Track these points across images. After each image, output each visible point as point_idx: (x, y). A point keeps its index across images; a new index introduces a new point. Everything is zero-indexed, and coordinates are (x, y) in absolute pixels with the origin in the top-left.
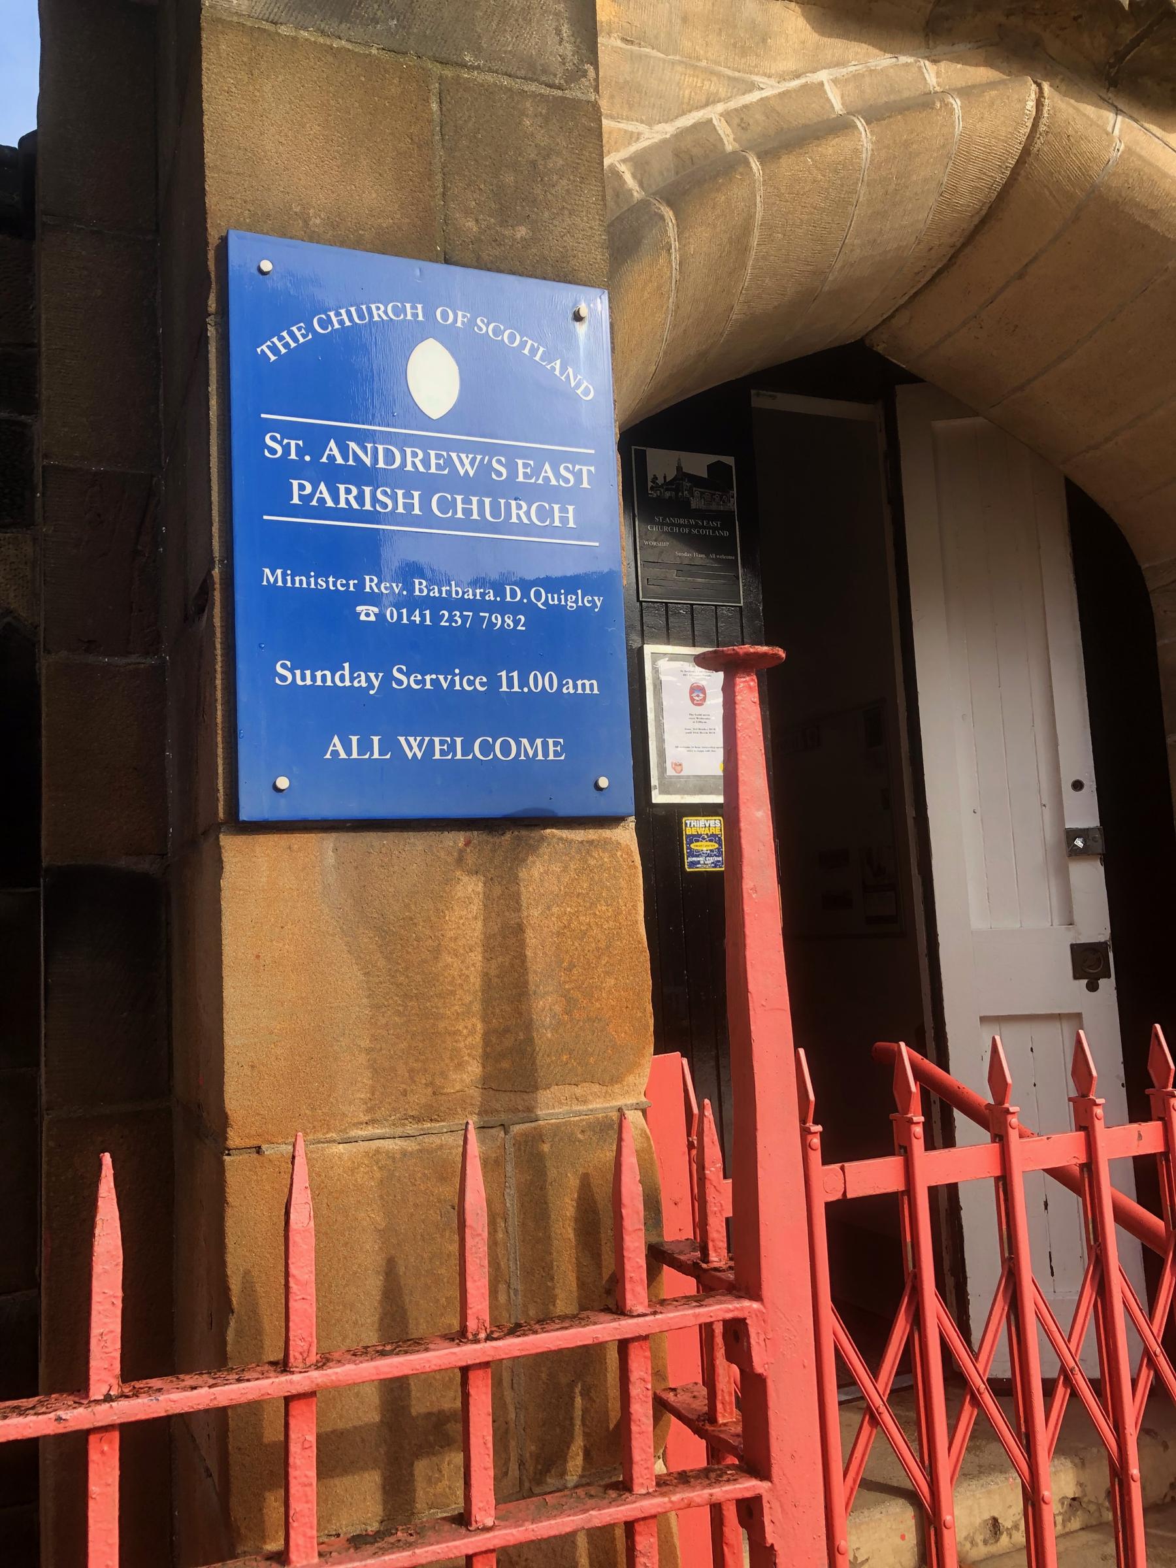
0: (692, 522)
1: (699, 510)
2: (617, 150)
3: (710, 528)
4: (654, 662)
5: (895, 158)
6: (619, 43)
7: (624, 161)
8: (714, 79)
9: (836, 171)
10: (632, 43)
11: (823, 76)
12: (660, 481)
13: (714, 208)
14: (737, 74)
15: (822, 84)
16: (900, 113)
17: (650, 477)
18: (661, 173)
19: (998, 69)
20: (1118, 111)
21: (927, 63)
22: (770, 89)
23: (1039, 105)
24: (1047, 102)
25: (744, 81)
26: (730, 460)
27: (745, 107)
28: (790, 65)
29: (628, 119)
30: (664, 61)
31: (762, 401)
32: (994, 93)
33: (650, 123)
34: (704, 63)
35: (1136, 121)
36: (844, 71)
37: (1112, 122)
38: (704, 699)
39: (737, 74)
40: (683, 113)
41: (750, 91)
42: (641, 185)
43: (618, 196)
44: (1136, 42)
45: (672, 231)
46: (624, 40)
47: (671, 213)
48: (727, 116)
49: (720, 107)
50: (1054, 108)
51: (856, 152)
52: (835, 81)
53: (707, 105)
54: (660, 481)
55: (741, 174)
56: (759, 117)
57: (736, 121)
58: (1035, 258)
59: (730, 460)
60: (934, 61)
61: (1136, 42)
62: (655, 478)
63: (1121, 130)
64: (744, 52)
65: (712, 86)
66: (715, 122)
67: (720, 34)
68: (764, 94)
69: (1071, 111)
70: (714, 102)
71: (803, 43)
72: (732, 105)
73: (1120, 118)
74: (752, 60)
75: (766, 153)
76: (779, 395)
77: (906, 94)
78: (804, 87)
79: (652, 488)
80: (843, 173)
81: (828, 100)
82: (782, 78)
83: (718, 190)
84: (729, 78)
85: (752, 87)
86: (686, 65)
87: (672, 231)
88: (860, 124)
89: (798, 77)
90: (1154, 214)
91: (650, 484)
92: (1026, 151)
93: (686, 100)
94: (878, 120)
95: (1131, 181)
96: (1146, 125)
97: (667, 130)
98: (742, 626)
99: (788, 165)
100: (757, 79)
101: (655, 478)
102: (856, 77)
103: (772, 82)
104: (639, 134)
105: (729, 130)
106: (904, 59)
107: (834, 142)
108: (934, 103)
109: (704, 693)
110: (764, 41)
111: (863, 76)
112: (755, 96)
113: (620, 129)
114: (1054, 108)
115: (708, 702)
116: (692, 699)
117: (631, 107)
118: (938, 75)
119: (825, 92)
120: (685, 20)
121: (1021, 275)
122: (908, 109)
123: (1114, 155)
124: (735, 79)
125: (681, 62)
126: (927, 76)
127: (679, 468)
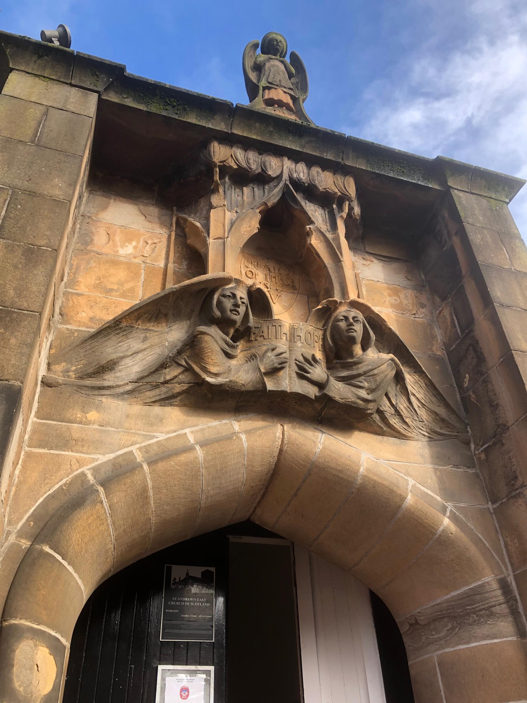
0: (191, 599)
1: (196, 594)
2: (87, 465)
3: (200, 602)
4: (162, 675)
5: (216, 458)
6: (97, 427)
7: (89, 469)
8: (137, 436)
9: (187, 465)
10: (103, 426)
11: (187, 431)
12: (177, 580)
13: (125, 484)
14: (147, 433)
15: (186, 434)
16: (217, 442)
17: (172, 578)
18: (105, 472)
19: (268, 421)
20: (323, 432)
21: (235, 422)
22: (162, 437)
23: (283, 434)
24: (286, 433)
25: (150, 436)
26: (213, 569)
27: (150, 445)
28: (173, 428)
29: (94, 453)
30: (115, 431)
31: (232, 539)
32: (261, 431)
33: (104, 454)
34: (133, 431)
35: (332, 436)
36: (196, 428)
37: (320, 438)
38: (188, 696)
39: (147, 433)
40: (120, 449)
41: (152, 439)
42: (95, 478)
43: (83, 483)
44: (323, 409)
45: (102, 495)
46: (100, 425)
47: (102, 489)
48: (140, 449)
49: (138, 446)
50: (289, 435)
51: (196, 458)
52: (192, 432)
53: (131, 445)
54: (177, 580)
55: (139, 471)
56: (155, 448)
57: (144, 450)
58: (299, 489)
59: (213, 569)
60: (238, 421)
61: (323, 409)
62: (175, 579)
63: (324, 440)
64: (152, 425)
65: (134, 439)
66: (134, 451)
67: (142, 419)
68: (158, 439)
69: (297, 435)
70: (135, 444)
71: (179, 420)
72: (143, 444)
73: (324, 435)
74: (155, 428)
75: (152, 462)
76: (243, 537)
77: (224, 434)
78: (177, 436)
79: (173, 584)
80: (191, 466)
81: (188, 439)
82: (168, 433)
83: (127, 478)
84: (143, 435)
85: (154, 437)
86: (125, 432)
87: (102, 495)
88: (198, 447)
89: (175, 432)
90: (341, 471)
91: (172, 582)
92: (281, 451)
93: (122, 445)
94: (206, 445)
95: (327, 459)
96: (336, 437)
97: (112, 456)
98: (213, 653)
99: (161, 466)
100: (155, 434)
101: (175, 579)
102: (201, 430)
103: (163, 435)
104: (98, 459)
105: (140, 454)
106: (224, 422)
107: (184, 455)
108: (233, 437)
109: (188, 691)
110: (161, 421)
111: (205, 429)
112: (155, 440)
113: (90, 458)
114: (289, 435)
115: (189, 697)
116: (181, 696)
117: (97, 449)
118: (240, 426)
119: (187, 436)
120: (127, 416)
121: (296, 495)
122: (220, 440)
123: (318, 450)
124: (147, 435)
125: (122, 431)
126: (234, 427)
127: (187, 574)
